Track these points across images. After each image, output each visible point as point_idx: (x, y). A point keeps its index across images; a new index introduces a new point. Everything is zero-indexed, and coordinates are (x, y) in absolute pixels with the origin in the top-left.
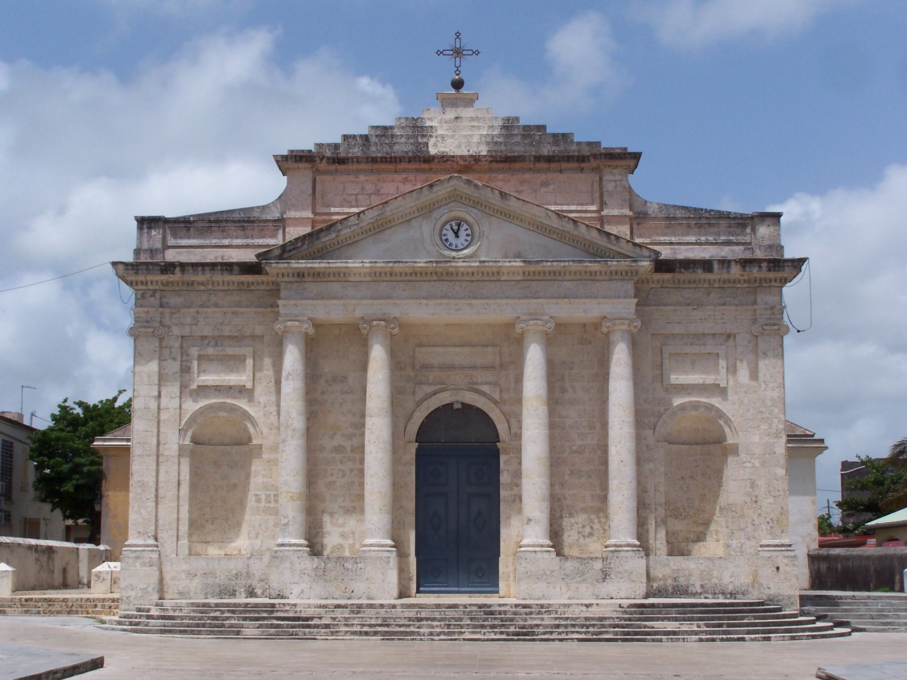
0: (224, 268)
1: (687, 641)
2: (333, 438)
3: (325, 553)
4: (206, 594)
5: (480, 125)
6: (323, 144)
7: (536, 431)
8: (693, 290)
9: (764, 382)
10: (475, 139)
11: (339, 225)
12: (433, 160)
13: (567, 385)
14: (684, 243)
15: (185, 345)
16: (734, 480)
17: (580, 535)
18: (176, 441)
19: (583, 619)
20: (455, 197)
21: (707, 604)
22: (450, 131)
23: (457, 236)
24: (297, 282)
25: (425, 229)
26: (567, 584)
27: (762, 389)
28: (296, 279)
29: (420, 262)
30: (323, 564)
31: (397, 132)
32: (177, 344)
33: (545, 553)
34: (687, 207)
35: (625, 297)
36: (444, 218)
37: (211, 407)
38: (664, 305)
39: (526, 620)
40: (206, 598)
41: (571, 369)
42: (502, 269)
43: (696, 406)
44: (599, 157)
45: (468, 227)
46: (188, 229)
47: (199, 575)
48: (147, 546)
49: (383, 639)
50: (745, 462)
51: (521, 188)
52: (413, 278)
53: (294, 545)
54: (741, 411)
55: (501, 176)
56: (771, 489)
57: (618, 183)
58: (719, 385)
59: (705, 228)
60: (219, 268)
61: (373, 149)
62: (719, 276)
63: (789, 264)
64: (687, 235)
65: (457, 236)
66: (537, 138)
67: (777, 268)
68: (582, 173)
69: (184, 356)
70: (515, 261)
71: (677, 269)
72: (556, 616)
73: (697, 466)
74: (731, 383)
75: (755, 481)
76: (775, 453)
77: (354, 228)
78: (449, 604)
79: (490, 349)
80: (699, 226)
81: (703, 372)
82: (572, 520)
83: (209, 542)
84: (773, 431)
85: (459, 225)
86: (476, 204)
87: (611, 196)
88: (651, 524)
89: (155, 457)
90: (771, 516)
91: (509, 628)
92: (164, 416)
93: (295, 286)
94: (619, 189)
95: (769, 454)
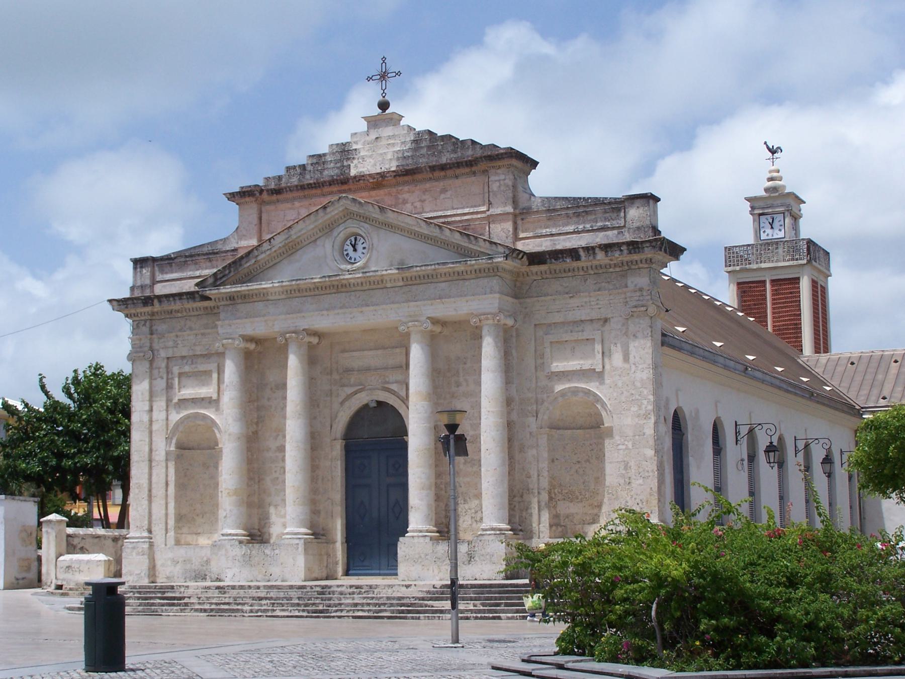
0: (188, 296)
1: (442, 619)
2: (276, 439)
3: (272, 541)
4: (185, 579)
5: (396, 142)
6: (269, 178)
7: (415, 425)
8: (571, 278)
9: (634, 364)
10: (389, 156)
11: (256, 251)
12: (348, 181)
13: (461, 379)
14: (563, 233)
15: (170, 365)
16: (611, 463)
17: (473, 520)
18: (164, 448)
19: (385, 599)
20: (348, 215)
21: (517, 584)
22: (370, 151)
23: (355, 250)
24: (231, 304)
25: (327, 248)
26: (438, 566)
27: (633, 371)
28: (229, 302)
29: (315, 278)
30: (249, 551)
31: (329, 158)
32: (163, 365)
33: (421, 538)
34: (566, 198)
35: (491, 293)
36: (342, 236)
37: (188, 417)
38: (545, 296)
39: (340, 599)
40: (185, 582)
41: (465, 363)
42: (384, 277)
43: (575, 391)
44: (480, 160)
45: (345, 246)
46: (170, 265)
47: (180, 562)
48: (142, 538)
49: (208, 615)
50: (619, 444)
51: (424, 197)
52: (317, 292)
53: (230, 535)
54: (615, 394)
55: (406, 188)
56: (641, 470)
57: (502, 182)
58: (595, 369)
59: (583, 217)
60: (185, 297)
61: (308, 177)
62: (590, 263)
63: (648, 245)
64: (567, 224)
65: (355, 250)
66: (440, 148)
67: (637, 250)
68: (475, 176)
69: (170, 375)
70: (390, 269)
71: (548, 260)
72: (373, 596)
73: (592, 450)
74: (607, 367)
75: (628, 463)
76: (644, 434)
77: (268, 253)
78: (299, 586)
79: (398, 350)
80: (578, 215)
81: (581, 358)
82: (466, 506)
83: (199, 533)
84: (642, 412)
85: (356, 239)
86: (366, 219)
87: (496, 196)
88: (535, 508)
89: (147, 463)
90: (641, 497)
91: (318, 607)
92: (155, 427)
93: (230, 308)
94: (502, 188)
95: (639, 436)
